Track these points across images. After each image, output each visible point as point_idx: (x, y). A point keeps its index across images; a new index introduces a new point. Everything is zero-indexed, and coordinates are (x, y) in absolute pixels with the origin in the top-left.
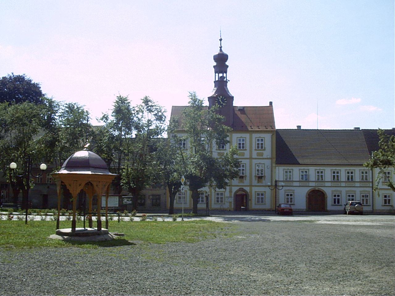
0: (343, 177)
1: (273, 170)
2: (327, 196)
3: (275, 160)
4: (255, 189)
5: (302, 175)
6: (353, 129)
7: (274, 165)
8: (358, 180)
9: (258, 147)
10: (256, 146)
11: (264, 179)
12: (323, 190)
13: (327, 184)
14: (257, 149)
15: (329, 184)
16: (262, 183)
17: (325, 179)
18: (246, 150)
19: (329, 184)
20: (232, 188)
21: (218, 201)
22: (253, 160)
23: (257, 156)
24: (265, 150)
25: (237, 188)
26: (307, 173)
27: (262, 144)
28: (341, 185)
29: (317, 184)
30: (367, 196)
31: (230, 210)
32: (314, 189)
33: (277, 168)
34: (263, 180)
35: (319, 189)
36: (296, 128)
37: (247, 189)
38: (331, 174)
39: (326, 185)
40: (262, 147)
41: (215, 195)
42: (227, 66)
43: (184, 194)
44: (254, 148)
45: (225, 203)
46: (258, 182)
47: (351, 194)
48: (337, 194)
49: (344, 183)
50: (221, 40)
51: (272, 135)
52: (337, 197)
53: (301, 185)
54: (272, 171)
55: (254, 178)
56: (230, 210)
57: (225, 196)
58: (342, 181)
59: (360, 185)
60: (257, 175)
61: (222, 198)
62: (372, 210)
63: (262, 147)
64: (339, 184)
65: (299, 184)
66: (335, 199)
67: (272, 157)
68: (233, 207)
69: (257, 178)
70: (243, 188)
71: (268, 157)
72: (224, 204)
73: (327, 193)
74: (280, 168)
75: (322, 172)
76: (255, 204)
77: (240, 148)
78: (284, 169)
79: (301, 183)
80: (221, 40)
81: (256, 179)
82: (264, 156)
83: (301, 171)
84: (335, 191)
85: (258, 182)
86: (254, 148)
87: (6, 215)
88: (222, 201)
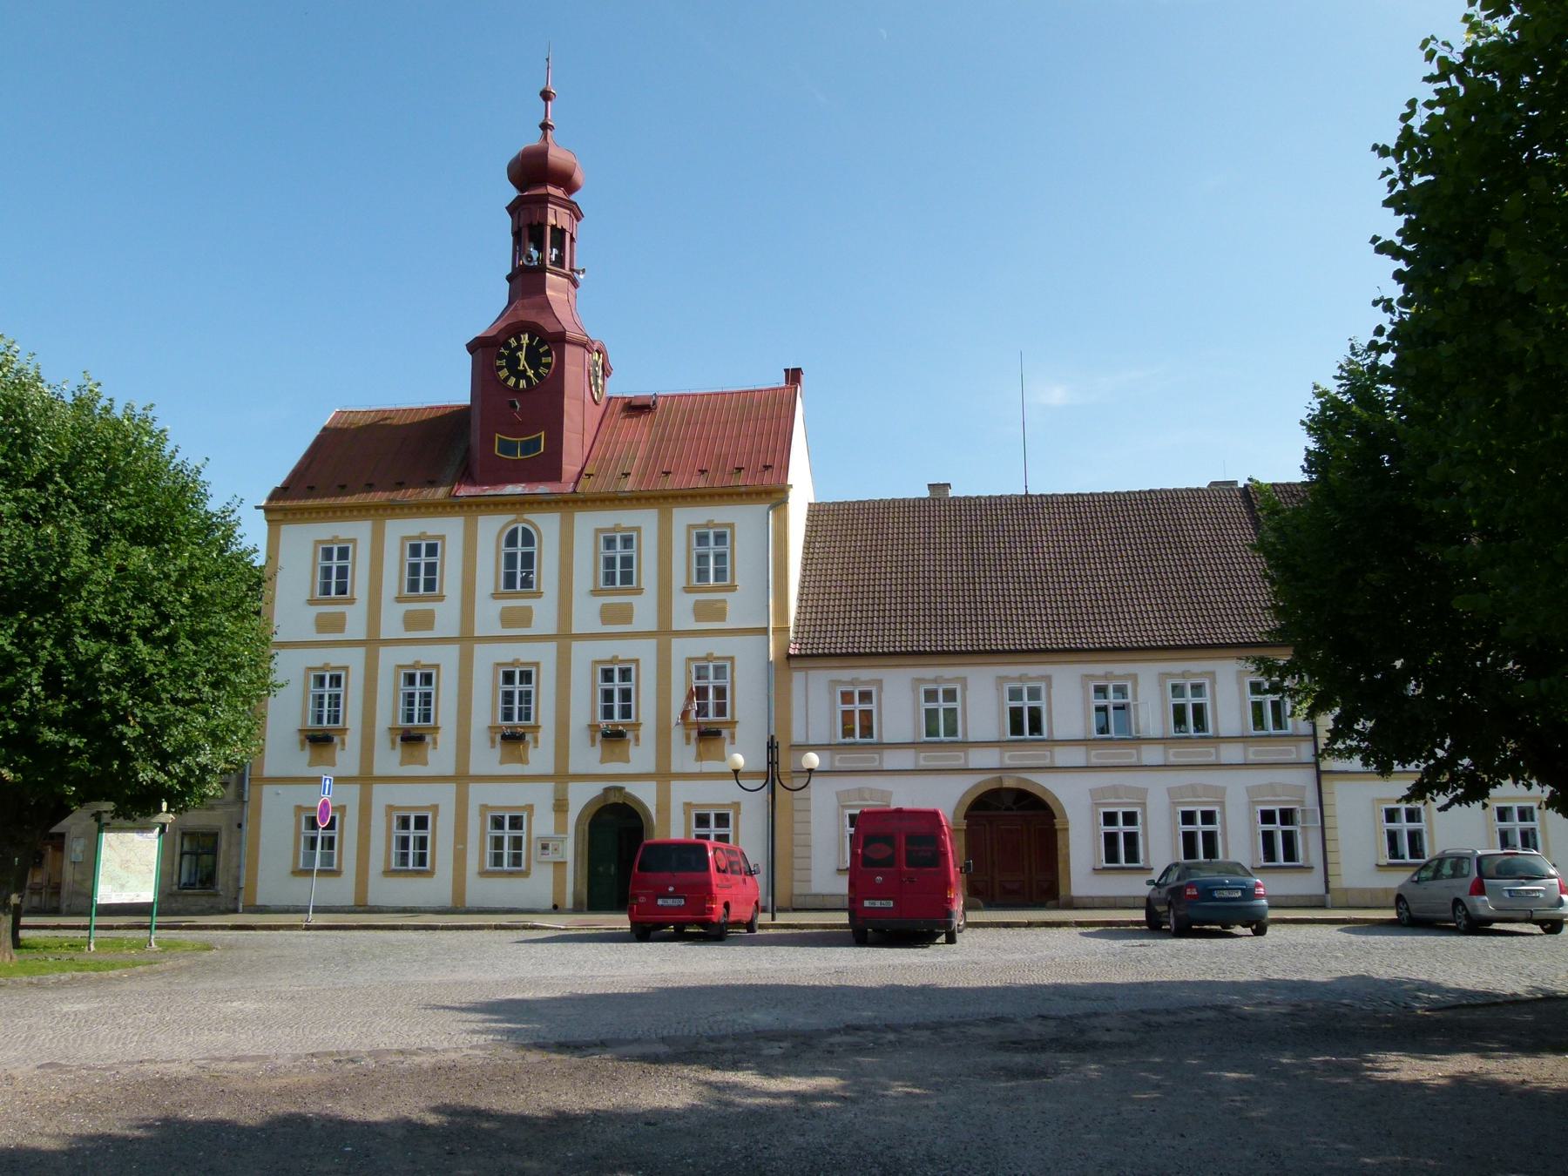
0: (1152, 715)
2: (1067, 822)
4: (681, 793)
5: (1102, 709)
6: (1205, 486)
8: (1077, 732)
12: (1045, 790)
13: (1063, 756)
14: (694, 582)
15: (1076, 756)
17: (965, 734)
18: (639, 591)
19: (1076, 756)
20: (565, 790)
22: (677, 644)
25: (594, 790)
26: (1124, 695)
29: (1009, 758)
30: (1287, 816)
32: (995, 786)
34: (339, 747)
35: (1023, 786)
36: (926, 494)
37: (645, 794)
38: (1242, 699)
39: (1058, 763)
42: (1398, 283)
43: (313, 841)
49: (1160, 747)
55: (677, 734)
58: (971, 739)
59: (1245, 754)
61: (517, 843)
62: (1321, 891)
63: (720, 575)
64: (1128, 755)
65: (1088, 754)
73: (1069, 811)
75: (866, 696)
77: (613, 583)
79: (1251, 750)
84: (1114, 790)
86: (679, 578)
87: (762, 927)
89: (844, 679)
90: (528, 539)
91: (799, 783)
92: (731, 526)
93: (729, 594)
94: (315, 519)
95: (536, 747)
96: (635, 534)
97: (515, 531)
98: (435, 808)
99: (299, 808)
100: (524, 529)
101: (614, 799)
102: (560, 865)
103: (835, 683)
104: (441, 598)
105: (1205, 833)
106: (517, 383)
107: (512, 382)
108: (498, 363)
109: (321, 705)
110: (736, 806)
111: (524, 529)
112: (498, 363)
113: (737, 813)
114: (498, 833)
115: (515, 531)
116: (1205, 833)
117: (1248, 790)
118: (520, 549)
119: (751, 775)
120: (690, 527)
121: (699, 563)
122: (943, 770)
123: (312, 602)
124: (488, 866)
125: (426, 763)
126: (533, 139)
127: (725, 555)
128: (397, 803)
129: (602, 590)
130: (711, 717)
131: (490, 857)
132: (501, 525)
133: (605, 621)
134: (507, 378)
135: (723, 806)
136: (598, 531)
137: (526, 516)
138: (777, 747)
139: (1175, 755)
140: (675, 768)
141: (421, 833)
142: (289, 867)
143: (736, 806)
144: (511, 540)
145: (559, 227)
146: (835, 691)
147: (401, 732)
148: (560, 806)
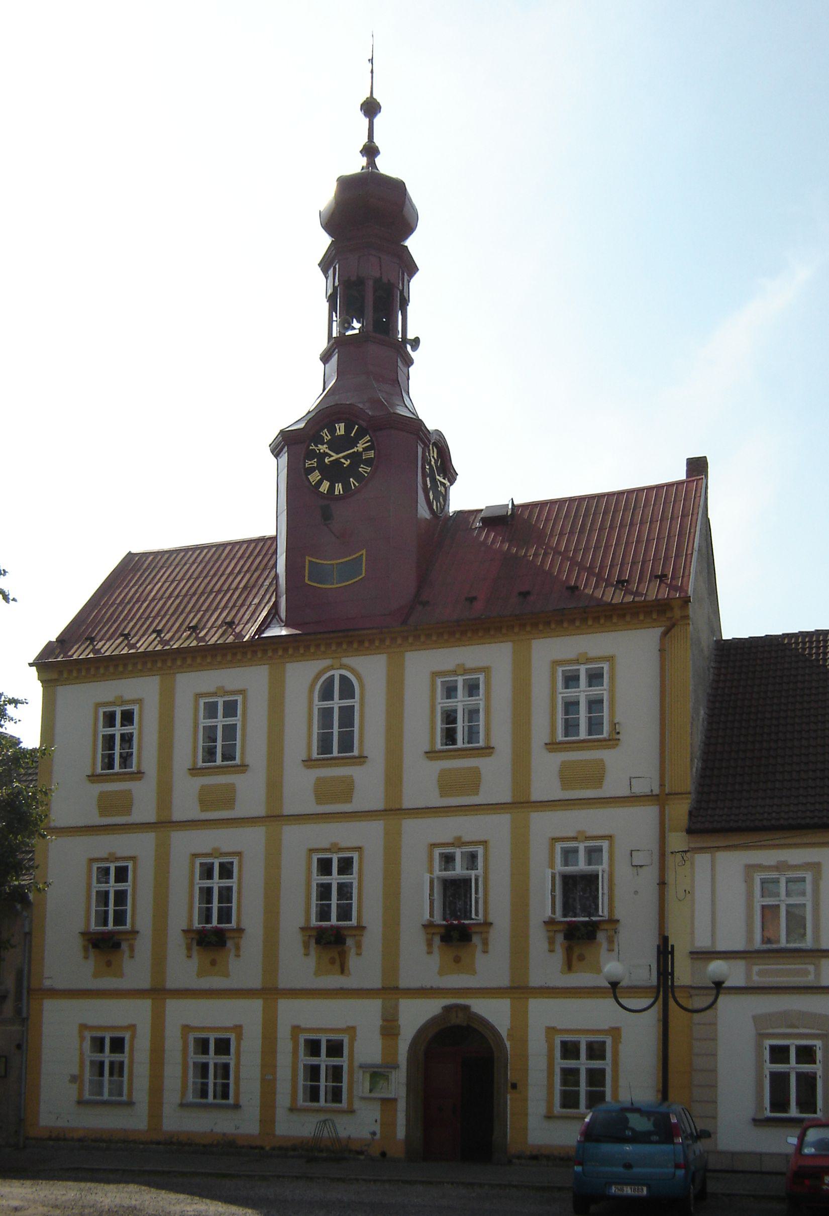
1: (670, 878)
3: (680, 810)
7: (677, 840)
9: (571, 727)
10: (195, 748)
11: (611, 941)
16: (227, 975)
17: (817, 937)
21: (314, 1095)
22: (411, 827)
23: (102, 814)
24: (613, 741)
25: (432, 1008)
27: (595, 704)
28: (818, 975)
31: (383, 1154)
33: (702, 860)
34: (127, 954)
40: (594, 725)
41: (295, 1052)
44: (540, 733)
45: (357, 1105)
46: (569, 966)
47: (793, 1044)
48: (793, 1044)
50: (371, 108)
51: (665, 634)
52: (793, 1066)
53: (757, 980)
54: (662, 883)
55: (538, 938)
56: (383, 1154)
57: (356, 1064)
60: (559, 916)
61: (336, 1073)
63: (594, 725)
66: (779, 1082)
67: (662, 785)
68: (401, 1133)
69: (560, 938)
70: (466, 1008)
71: (641, 788)
72: (351, 1111)
74: (723, 857)
76: (549, 1117)
78: (751, 869)
80: (371, 108)
81: (551, 941)
82: (614, 786)
83: (757, 878)
84: (785, 1018)
85: (569, 966)
86: (540, 733)
88: (336, 1095)
89: (766, 863)
90: (347, 690)
91: (699, 1002)
92: (610, 659)
93: (357, 768)
94: (190, 666)
95: (359, 954)
96: (481, 677)
97: (331, 679)
98: (238, 1029)
99: (84, 1027)
100: (343, 678)
101: (458, 1019)
102: (388, 1103)
103: (751, 869)
104: (361, 759)
105: (799, 1075)
106: (332, 488)
107: (325, 487)
108: (308, 464)
109: (209, 901)
110: (615, 1032)
111: (343, 678)
112: (308, 464)
113: (239, 1038)
114: (314, 1061)
115: (331, 679)
116: (799, 1075)
117: (755, 1018)
118: (336, 703)
119: (635, 990)
120: (556, 663)
121: (567, 712)
122: (771, 988)
123: (94, 778)
124: (190, 1098)
125: (227, 975)
126: (356, 165)
127: (601, 701)
128: (91, 1022)
129: (560, 743)
130: (111, 926)
131: (304, 1093)
132: (312, 675)
133: (444, 793)
134: (320, 483)
135: (599, 1032)
136: (435, 675)
137: (345, 661)
138: (672, 953)
139: (760, 973)
140: (535, 980)
141: (223, 1059)
142: (750, 1113)
143: (615, 1032)
144: (327, 694)
145: (385, 280)
146: (753, 879)
147: (314, 933)
148: (390, 1030)
